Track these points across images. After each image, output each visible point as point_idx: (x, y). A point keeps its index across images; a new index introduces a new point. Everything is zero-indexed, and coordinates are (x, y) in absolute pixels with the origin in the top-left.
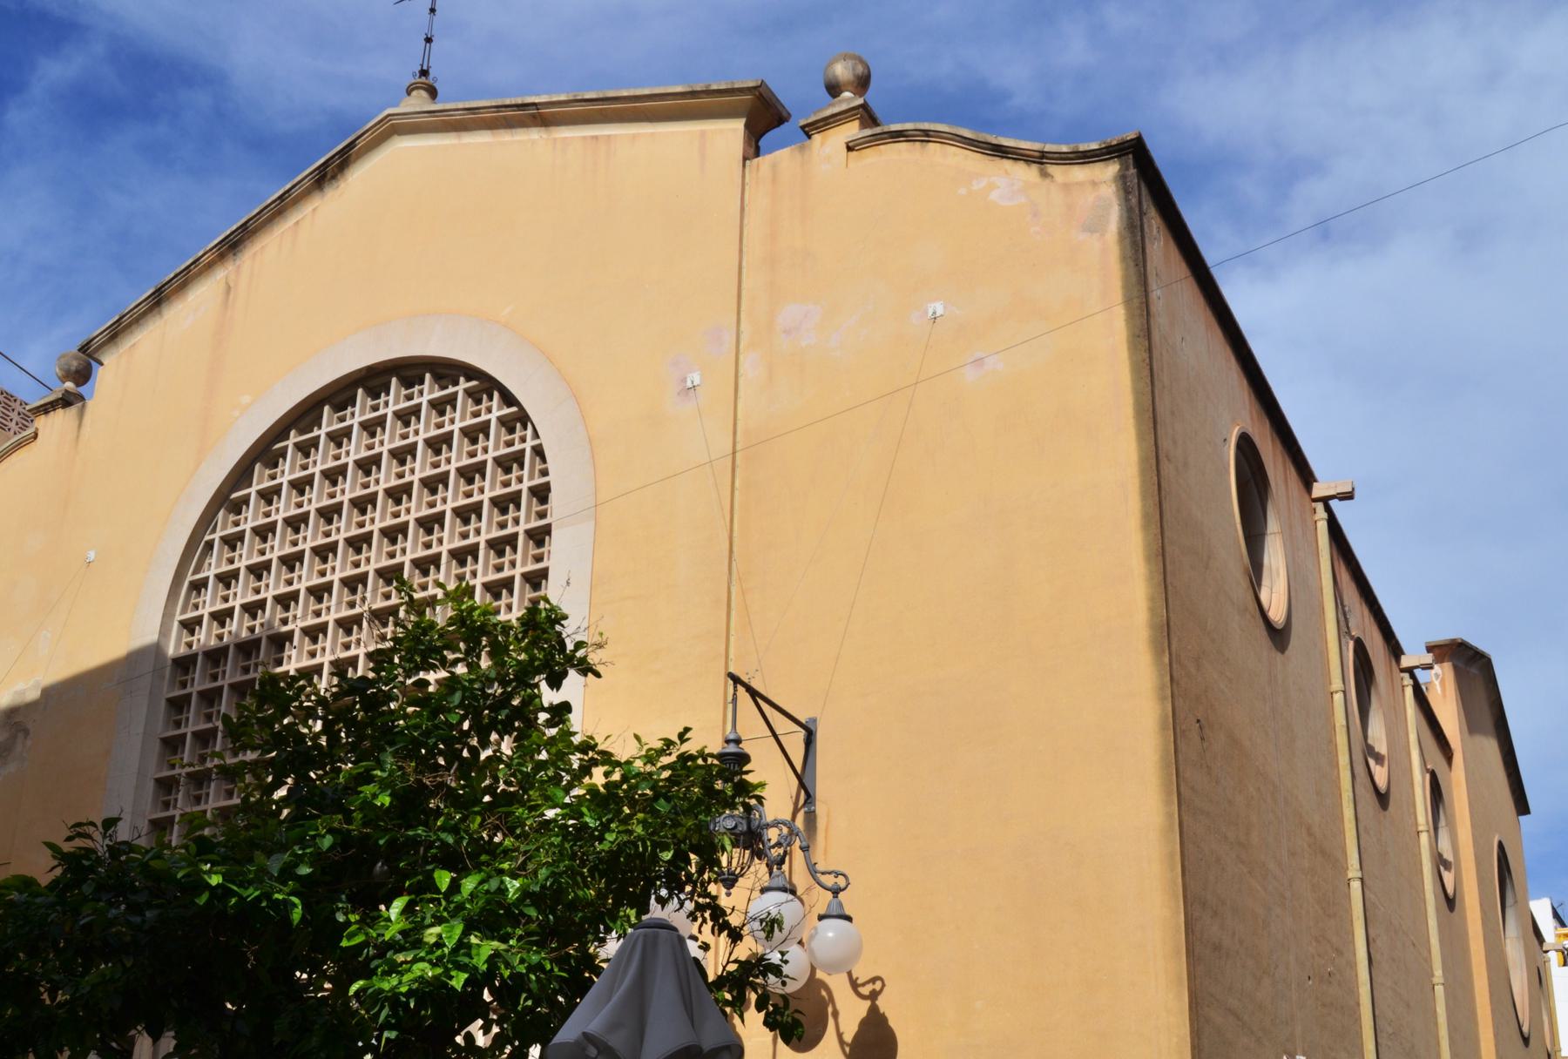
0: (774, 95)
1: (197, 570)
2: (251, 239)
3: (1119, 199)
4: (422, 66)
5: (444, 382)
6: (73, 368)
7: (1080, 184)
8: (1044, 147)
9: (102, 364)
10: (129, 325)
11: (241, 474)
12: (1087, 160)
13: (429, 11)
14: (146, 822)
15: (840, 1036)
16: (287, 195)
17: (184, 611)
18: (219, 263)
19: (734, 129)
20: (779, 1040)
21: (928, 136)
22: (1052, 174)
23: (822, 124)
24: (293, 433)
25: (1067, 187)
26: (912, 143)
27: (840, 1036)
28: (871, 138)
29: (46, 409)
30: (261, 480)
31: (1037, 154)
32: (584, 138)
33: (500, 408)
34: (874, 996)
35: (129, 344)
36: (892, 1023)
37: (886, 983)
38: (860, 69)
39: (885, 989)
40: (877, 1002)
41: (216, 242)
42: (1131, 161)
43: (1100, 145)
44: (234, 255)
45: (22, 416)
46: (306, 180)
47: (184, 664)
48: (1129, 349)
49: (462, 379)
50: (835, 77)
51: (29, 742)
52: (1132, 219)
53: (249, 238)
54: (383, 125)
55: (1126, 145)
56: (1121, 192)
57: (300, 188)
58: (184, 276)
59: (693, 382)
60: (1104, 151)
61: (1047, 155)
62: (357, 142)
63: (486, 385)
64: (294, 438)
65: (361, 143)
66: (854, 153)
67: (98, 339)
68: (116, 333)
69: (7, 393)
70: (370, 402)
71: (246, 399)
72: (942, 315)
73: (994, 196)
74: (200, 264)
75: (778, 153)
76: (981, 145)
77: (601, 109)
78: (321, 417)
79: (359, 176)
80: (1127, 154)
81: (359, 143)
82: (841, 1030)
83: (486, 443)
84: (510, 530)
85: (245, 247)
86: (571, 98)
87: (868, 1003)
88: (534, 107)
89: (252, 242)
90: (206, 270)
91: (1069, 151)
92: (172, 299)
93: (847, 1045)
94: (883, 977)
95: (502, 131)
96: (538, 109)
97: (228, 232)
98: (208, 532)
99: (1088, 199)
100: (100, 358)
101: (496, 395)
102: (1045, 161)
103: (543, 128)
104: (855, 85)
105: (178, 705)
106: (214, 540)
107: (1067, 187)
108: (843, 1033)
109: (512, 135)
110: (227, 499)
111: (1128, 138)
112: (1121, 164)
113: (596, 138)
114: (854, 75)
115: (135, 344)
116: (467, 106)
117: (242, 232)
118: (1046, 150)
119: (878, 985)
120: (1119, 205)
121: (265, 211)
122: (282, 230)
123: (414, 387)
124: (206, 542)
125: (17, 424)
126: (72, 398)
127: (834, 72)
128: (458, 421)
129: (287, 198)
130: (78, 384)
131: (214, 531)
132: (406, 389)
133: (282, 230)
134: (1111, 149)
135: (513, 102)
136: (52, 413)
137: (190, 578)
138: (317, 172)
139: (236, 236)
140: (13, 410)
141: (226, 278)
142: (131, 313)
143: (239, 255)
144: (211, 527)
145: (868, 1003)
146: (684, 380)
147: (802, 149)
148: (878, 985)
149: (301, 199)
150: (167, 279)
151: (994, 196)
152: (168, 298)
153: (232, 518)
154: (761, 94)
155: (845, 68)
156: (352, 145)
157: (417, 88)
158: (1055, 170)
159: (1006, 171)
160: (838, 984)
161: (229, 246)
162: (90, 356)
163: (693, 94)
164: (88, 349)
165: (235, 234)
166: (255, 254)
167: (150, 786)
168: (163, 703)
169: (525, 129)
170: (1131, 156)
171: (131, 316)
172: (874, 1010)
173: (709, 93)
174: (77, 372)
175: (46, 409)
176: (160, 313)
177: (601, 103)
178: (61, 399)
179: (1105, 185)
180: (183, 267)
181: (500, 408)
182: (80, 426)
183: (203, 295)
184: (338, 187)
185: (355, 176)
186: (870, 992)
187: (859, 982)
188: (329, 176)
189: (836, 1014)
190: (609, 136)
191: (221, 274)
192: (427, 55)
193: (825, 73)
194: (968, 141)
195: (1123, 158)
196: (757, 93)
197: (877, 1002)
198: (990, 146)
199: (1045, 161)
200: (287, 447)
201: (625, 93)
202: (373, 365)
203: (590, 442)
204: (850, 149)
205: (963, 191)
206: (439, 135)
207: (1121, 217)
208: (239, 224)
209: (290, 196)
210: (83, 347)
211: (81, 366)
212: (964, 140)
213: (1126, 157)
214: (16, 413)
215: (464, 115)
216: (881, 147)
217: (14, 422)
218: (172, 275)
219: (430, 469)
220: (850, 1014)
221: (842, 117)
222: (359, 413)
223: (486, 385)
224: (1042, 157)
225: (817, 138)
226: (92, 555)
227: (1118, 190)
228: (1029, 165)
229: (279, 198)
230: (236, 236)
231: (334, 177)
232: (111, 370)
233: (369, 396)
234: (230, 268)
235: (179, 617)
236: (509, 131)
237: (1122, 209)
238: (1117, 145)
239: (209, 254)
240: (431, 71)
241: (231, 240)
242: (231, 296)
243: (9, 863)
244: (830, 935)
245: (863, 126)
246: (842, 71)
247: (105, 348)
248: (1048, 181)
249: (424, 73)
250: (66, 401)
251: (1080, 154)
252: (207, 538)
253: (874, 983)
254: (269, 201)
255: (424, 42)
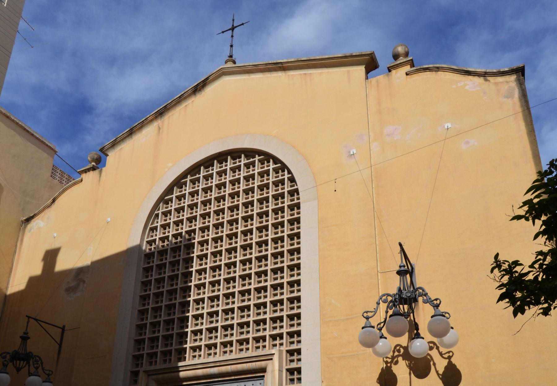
0: (376, 58)
1: (152, 224)
2: (167, 112)
3: (518, 87)
4: (230, 54)
5: (248, 158)
6: (95, 158)
7: (501, 83)
8: (486, 70)
9: (108, 155)
10: (120, 141)
11: (169, 190)
12: (503, 75)
13: (231, 37)
14: (137, 311)
15: (437, 372)
16: (182, 96)
17: (148, 238)
18: (155, 120)
19: (361, 69)
20: (412, 375)
21: (438, 69)
22: (489, 80)
23: (396, 66)
24: (189, 176)
25: (496, 84)
26: (431, 72)
27: (437, 372)
28: (416, 70)
29: (86, 171)
30: (176, 192)
31: (483, 73)
32: (301, 74)
33: (273, 165)
34: (449, 358)
35: (120, 148)
36: (458, 367)
37: (454, 353)
38: (407, 49)
39: (454, 355)
40: (451, 360)
41: (154, 112)
42: (521, 74)
43: (509, 69)
44: (161, 117)
45: (67, 179)
46: (190, 91)
47: (149, 256)
48: (528, 136)
49: (257, 156)
50: (398, 52)
51: (85, 285)
52: (524, 93)
53: (167, 111)
54: (219, 72)
55: (519, 69)
56: (519, 85)
57: (187, 93)
58: (141, 124)
59: (353, 153)
60: (511, 71)
61: (488, 73)
62: (209, 78)
63: (267, 158)
64: (189, 178)
65: (211, 78)
66: (409, 76)
67: (107, 146)
68: (114, 144)
69: (62, 171)
70: (219, 165)
71: (170, 165)
72: (450, 128)
73: (467, 88)
74: (148, 120)
75: (378, 77)
76: (460, 71)
77: (308, 64)
78: (200, 171)
79: (209, 90)
80: (519, 72)
81: (210, 78)
82: (437, 370)
83: (196, 223)
84: (205, 252)
85: (165, 114)
86: (296, 60)
87: (447, 360)
88: (281, 64)
89: (168, 112)
90: (150, 122)
91: (497, 71)
92: (136, 132)
93: (441, 375)
94: (453, 351)
95: (267, 73)
96: (282, 64)
97: (159, 109)
98: (156, 211)
99: (506, 87)
100: (107, 153)
101: (271, 161)
102: (486, 75)
103: (283, 72)
104: (405, 55)
105: (147, 270)
106: (159, 213)
107: (496, 84)
108: (438, 371)
109: (271, 74)
110: (164, 199)
111: (520, 66)
112: (517, 75)
113: (305, 74)
114: (405, 51)
115: (121, 148)
116: (254, 64)
117: (164, 109)
118: (487, 71)
119: (451, 354)
120: (518, 89)
121: (173, 102)
122: (180, 109)
123: (236, 159)
124: (156, 214)
125: (66, 182)
126: (96, 167)
127: (398, 50)
128: (257, 169)
129: (182, 97)
130: (96, 164)
131: (159, 210)
132: (233, 160)
133: (180, 109)
134: (513, 70)
135: (273, 62)
136: (88, 172)
137: (150, 226)
138: (194, 88)
139: (163, 110)
140: (64, 177)
141: (158, 125)
142: (120, 137)
143: (163, 117)
144: (158, 207)
145: (447, 360)
146: (350, 152)
147: (388, 75)
148: (451, 354)
149: (187, 98)
150: (135, 125)
151: (467, 88)
152: (135, 132)
153: (165, 206)
154: (372, 57)
155: (402, 49)
156: (207, 79)
157: (230, 61)
158: (491, 79)
159: (471, 80)
160: (434, 353)
161: (159, 114)
162: (103, 153)
163: (346, 57)
164: (103, 150)
165: (162, 110)
166: (169, 117)
167: (138, 298)
168: (141, 269)
169: (276, 72)
170: (520, 73)
171: (120, 138)
172: (450, 363)
173: (352, 56)
174: (97, 159)
175: (85, 171)
176: (131, 137)
177: (308, 61)
178: (92, 167)
179: (512, 83)
180: (141, 121)
181: (273, 165)
182: (100, 176)
183: (149, 132)
184: (201, 94)
185: (208, 90)
186: (448, 356)
187: (443, 353)
188: (198, 90)
189: (434, 364)
190: (310, 73)
191: (155, 124)
192: (231, 51)
193: (394, 49)
194: (455, 70)
195: (517, 73)
196: (371, 56)
197: (451, 360)
198: (464, 71)
199: (486, 75)
200: (187, 181)
201: (318, 58)
202: (221, 152)
203: (313, 174)
204: (407, 74)
205: (454, 87)
206: (242, 75)
207: (519, 93)
208: (163, 106)
209: (183, 96)
210: (101, 149)
211: (98, 157)
212: (453, 70)
213: (519, 73)
214: (65, 178)
215: (252, 67)
216: (419, 73)
217: (65, 181)
218: (137, 124)
219: (175, 231)
220: (441, 364)
221: (404, 64)
222: (216, 168)
223: (267, 158)
224: (485, 74)
225: (393, 72)
226: (109, 219)
227: (517, 84)
228: (479, 77)
229: (179, 97)
230: (163, 110)
231: (200, 90)
232: (112, 157)
233: (218, 163)
234: (159, 122)
235: (146, 240)
236: (269, 73)
237: (519, 90)
238: (516, 69)
239: (151, 117)
240: (233, 56)
241: (160, 112)
242: (161, 131)
243: (79, 328)
244: (418, 344)
245: (411, 67)
246: (400, 49)
247: (110, 149)
248: (487, 82)
249: (231, 56)
250: (94, 169)
251: (501, 72)
252: (156, 212)
253: (449, 353)
254: (175, 98)
255: (230, 47)
